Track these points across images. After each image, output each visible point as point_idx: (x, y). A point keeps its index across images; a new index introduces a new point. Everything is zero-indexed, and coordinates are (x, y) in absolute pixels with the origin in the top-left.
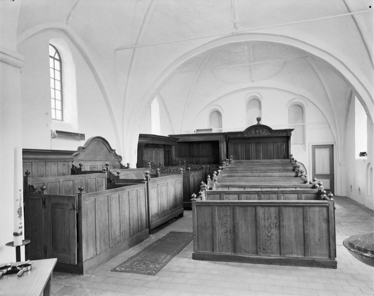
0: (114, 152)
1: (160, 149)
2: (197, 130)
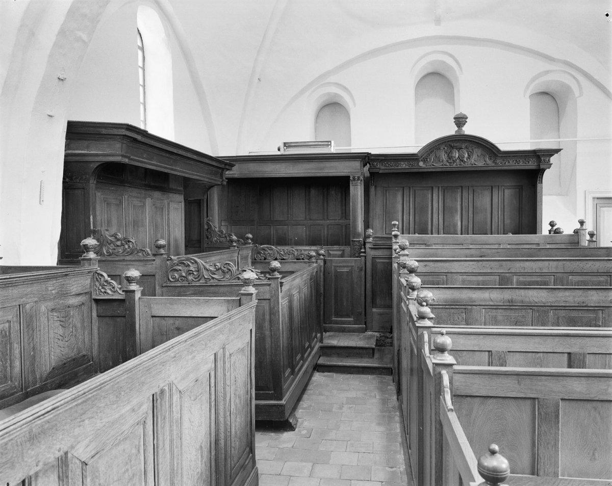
1: (171, 195)
2: (285, 144)
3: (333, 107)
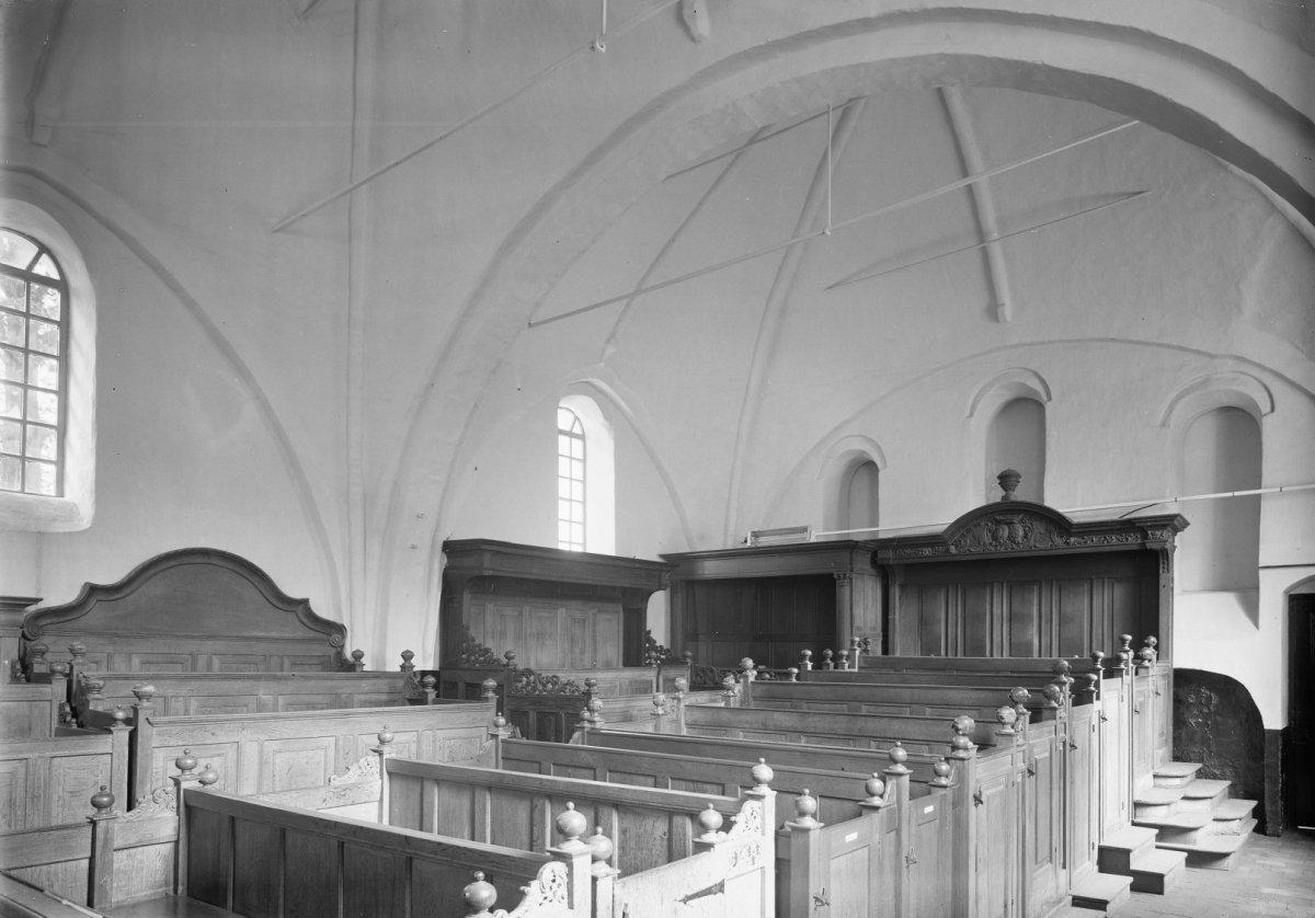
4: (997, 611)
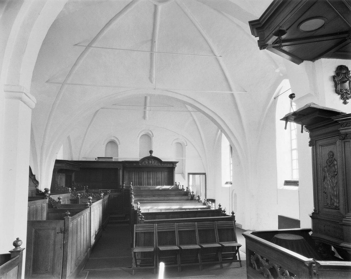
0: (33, 177)
3: (113, 143)
4: (145, 176)
